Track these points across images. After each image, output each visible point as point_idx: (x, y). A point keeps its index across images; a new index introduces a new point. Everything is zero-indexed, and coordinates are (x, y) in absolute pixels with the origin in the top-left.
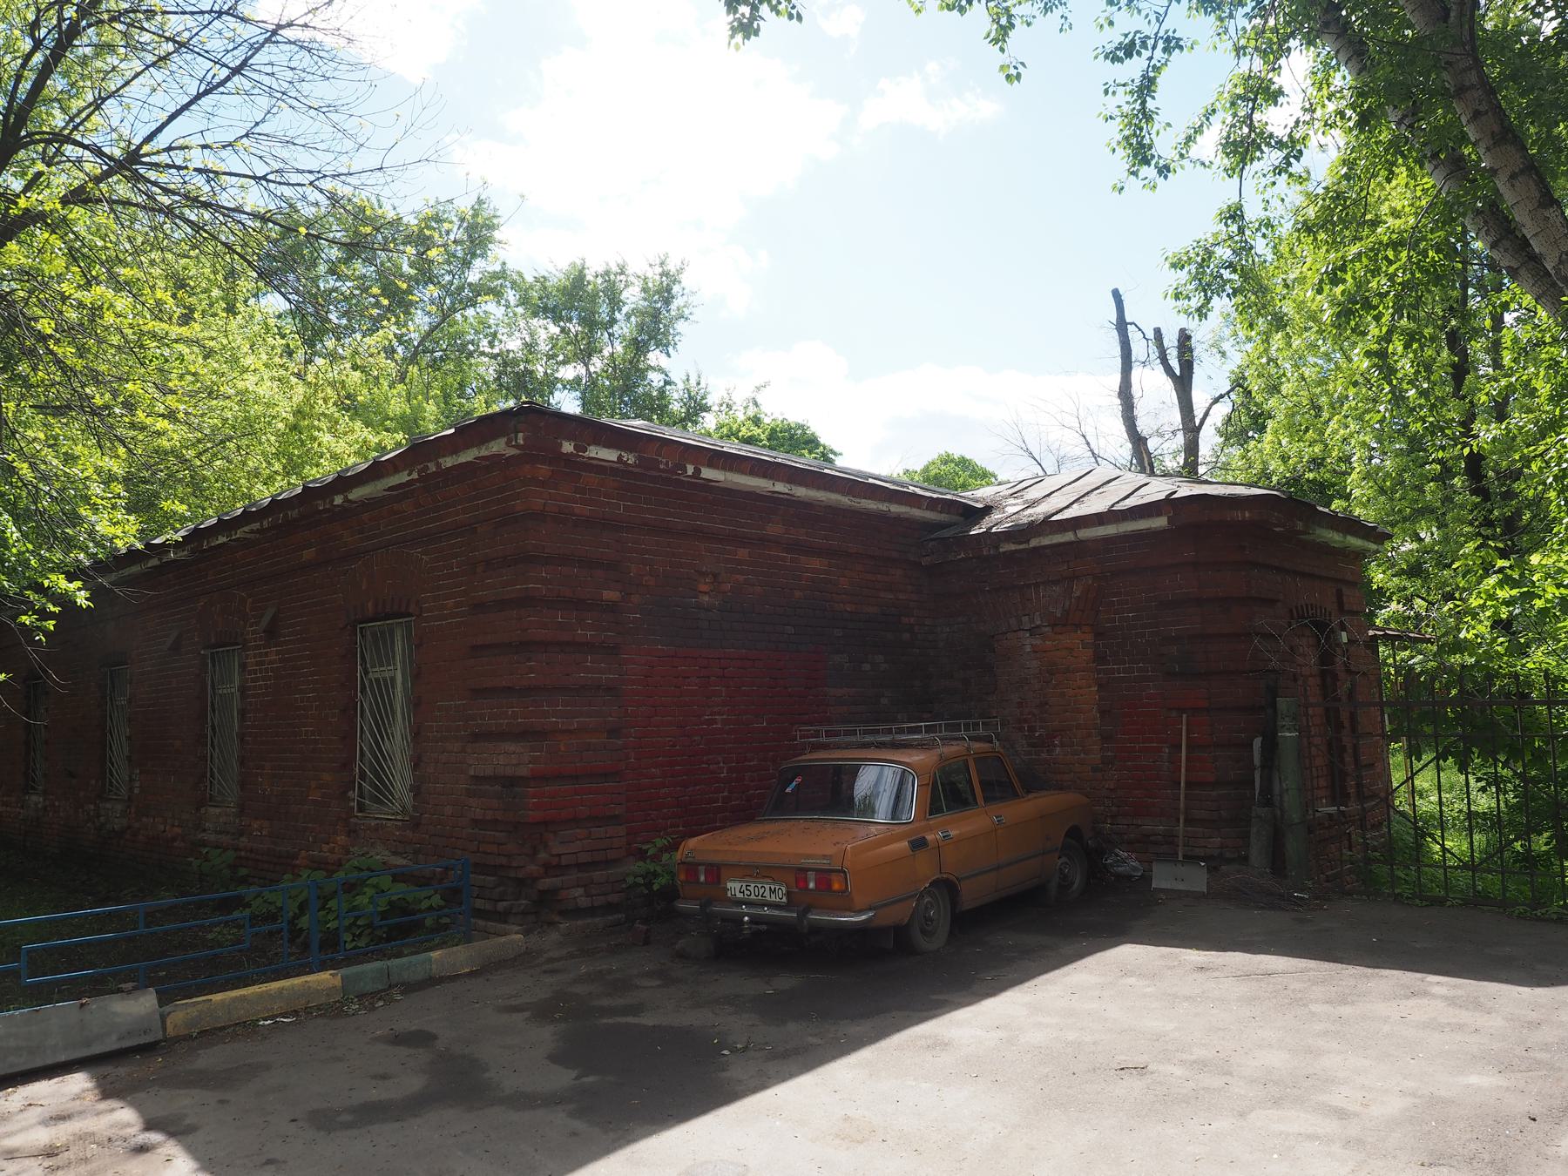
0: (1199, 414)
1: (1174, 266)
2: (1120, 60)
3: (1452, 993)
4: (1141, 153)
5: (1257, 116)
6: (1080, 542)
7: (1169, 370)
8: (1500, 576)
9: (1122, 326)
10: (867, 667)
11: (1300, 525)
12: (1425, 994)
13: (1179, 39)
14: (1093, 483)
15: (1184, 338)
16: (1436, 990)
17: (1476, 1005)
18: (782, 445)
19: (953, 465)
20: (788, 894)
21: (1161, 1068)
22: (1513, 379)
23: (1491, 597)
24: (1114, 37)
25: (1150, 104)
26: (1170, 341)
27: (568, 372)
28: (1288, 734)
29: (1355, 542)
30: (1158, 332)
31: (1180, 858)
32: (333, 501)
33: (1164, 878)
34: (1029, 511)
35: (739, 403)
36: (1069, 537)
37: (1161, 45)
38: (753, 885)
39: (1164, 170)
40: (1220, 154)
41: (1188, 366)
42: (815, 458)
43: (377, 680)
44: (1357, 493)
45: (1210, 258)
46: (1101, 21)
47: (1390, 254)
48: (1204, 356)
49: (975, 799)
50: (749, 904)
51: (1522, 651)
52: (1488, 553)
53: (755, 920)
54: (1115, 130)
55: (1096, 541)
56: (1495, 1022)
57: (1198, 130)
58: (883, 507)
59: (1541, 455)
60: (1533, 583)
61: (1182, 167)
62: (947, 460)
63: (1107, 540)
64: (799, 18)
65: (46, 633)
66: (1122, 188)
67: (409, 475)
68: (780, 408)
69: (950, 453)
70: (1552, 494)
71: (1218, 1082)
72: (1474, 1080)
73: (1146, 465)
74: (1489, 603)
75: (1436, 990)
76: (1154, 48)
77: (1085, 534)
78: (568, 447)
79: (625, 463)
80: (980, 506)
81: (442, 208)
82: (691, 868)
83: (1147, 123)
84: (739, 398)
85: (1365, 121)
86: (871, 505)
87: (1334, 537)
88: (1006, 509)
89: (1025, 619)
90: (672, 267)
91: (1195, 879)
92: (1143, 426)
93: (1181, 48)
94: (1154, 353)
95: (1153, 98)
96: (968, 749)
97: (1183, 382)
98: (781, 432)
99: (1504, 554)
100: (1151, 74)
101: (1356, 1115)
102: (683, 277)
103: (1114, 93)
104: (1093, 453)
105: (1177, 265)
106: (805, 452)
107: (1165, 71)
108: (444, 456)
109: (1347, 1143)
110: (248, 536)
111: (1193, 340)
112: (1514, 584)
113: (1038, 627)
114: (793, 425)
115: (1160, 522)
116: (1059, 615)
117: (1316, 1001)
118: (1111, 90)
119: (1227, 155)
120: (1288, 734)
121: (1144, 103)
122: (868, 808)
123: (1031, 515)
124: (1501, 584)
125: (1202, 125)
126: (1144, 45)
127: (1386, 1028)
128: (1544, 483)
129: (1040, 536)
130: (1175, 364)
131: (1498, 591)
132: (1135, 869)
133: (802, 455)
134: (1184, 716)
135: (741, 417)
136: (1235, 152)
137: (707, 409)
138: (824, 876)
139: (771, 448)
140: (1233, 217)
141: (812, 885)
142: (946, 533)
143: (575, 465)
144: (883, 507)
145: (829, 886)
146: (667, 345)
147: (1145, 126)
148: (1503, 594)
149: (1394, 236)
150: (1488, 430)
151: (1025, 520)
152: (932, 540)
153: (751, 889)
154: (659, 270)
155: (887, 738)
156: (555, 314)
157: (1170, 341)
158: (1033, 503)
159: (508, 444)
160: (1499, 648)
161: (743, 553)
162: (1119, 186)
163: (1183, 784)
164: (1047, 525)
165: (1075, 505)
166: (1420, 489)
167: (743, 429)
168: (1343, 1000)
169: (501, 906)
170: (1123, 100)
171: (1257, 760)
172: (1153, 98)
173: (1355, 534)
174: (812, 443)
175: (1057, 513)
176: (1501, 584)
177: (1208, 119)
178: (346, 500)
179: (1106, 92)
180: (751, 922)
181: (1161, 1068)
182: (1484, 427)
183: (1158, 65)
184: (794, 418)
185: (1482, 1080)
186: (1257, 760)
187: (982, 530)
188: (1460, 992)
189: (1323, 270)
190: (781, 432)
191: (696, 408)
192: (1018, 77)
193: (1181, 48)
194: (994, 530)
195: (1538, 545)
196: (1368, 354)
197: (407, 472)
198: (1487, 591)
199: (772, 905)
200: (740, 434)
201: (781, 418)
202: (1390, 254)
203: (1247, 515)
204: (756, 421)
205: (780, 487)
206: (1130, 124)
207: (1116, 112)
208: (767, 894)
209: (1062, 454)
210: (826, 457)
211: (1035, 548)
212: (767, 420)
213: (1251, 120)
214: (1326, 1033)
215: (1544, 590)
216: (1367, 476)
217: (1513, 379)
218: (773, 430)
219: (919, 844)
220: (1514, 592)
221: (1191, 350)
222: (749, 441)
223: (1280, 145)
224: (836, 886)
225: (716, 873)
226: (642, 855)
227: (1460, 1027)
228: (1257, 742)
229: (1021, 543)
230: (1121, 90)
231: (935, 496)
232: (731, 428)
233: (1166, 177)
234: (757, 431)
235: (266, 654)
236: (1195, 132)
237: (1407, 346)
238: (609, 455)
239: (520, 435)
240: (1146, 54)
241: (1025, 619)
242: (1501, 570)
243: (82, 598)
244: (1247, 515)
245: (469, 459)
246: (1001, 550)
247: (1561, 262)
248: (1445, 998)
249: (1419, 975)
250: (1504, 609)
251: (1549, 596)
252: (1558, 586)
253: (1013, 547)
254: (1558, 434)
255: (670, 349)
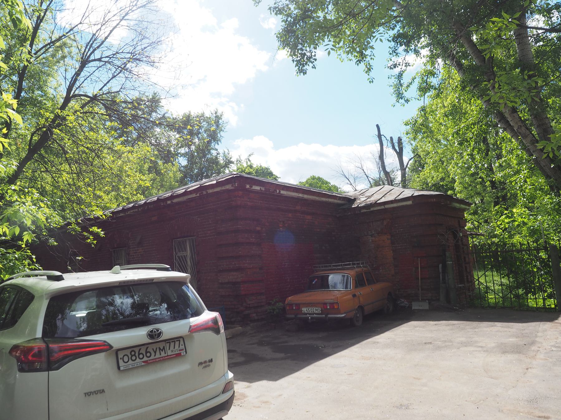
0: (405, 164)
1: (406, 125)
2: (392, 69)
3: (502, 325)
4: (400, 96)
5: (428, 80)
6: (386, 209)
7: (395, 150)
8: (506, 216)
9: (380, 136)
10: (324, 248)
11: (448, 202)
12: (495, 326)
13: (409, 63)
14: (386, 191)
15: (400, 140)
16: (498, 325)
17: (509, 327)
18: (260, 175)
19: (316, 180)
20: (322, 310)
21: (435, 342)
22: (506, 159)
23: (503, 221)
24: (391, 63)
25: (402, 82)
26: (395, 141)
27: (182, 151)
28: (449, 263)
29: (463, 206)
30: (391, 138)
31: (420, 300)
32: (167, 202)
33: (416, 306)
34: (368, 200)
35: (243, 160)
36: (382, 207)
37: (404, 65)
38: (310, 309)
39: (407, 101)
40: (418, 91)
41: (401, 149)
42: (272, 179)
43: (182, 256)
44: (457, 189)
45: (416, 122)
46: (388, 59)
47: (472, 126)
48: (406, 146)
49: (365, 283)
50: (309, 314)
51: (511, 237)
52: (502, 209)
53: (312, 318)
54: (392, 90)
55: (390, 208)
56: (514, 330)
57: (411, 83)
58: (327, 200)
59: (515, 180)
60: (515, 217)
61: (412, 100)
62: (313, 178)
63: (394, 208)
64: (315, 68)
65: (94, 244)
66: (395, 106)
67: (196, 195)
68: (258, 162)
69: (315, 175)
70: (519, 192)
71: (450, 344)
72: (511, 340)
73: (389, 181)
74: (503, 223)
75: (498, 325)
76: (402, 65)
77: (387, 206)
78: (248, 186)
79: (262, 190)
80: (353, 198)
81: (141, 96)
82: (291, 305)
83: (401, 87)
84: (243, 158)
85: (463, 88)
86: (324, 199)
87: (457, 205)
88: (361, 199)
89: (369, 232)
90: (218, 114)
91: (425, 306)
92: (388, 169)
93: (410, 66)
94: (390, 145)
95: (402, 79)
96: (363, 270)
97: (400, 154)
98: (260, 170)
99: (507, 209)
100: (402, 73)
101: (485, 347)
102: (223, 117)
103: (391, 78)
104: (367, 176)
105: (406, 124)
106: (268, 177)
107: (406, 72)
108: (209, 189)
109: (484, 351)
110: (131, 213)
111: (403, 141)
112: (510, 218)
113: (374, 234)
114: (264, 168)
115: (410, 203)
116: (380, 230)
117: (468, 329)
118: (390, 77)
119: (420, 92)
120: (449, 263)
121: (400, 81)
122: (335, 286)
123: (370, 201)
124: (506, 218)
125: (412, 82)
126: (399, 65)
127: (487, 332)
128: (516, 189)
129: (374, 207)
130: (397, 148)
131: (505, 220)
132: (406, 304)
133: (267, 178)
134: (419, 259)
135: (245, 165)
136: (422, 91)
137: (232, 163)
138: (332, 304)
139: (257, 176)
140: (422, 110)
141: (328, 307)
142: (345, 207)
143: (250, 191)
144: (327, 200)
145: (334, 307)
146: (218, 141)
147: (400, 88)
148: (506, 221)
149: (473, 122)
150: (500, 173)
151: (369, 203)
152: (340, 209)
153: (310, 310)
154: (215, 115)
155: (330, 268)
156: (179, 131)
157: (395, 141)
158: (369, 197)
159: (232, 186)
160: (506, 236)
161: (290, 215)
162: (394, 105)
163: (420, 278)
164: (376, 204)
165: (383, 198)
166: (475, 187)
167: (247, 170)
168: (475, 328)
169: (233, 320)
170: (394, 81)
171: (440, 270)
172: (402, 79)
173: (463, 204)
174: (271, 174)
175: (378, 200)
176: (506, 218)
177: (413, 80)
178: (172, 202)
179: (389, 78)
180: (311, 319)
181: (435, 342)
182: (499, 172)
183: (403, 70)
184: (264, 165)
185: (513, 340)
186: (440, 270)
187: (356, 206)
188: (504, 325)
189: (454, 131)
190: (260, 170)
191: (229, 162)
192: (372, 82)
193: (410, 66)
194: (359, 206)
195: (514, 205)
196: (468, 155)
197: (195, 194)
198: (502, 220)
199: (316, 314)
200: (246, 171)
201: (259, 165)
202: (472, 126)
203: (434, 200)
204: (251, 167)
205: (301, 195)
206: (396, 87)
207: (392, 84)
208: (315, 311)
209: (356, 176)
210: (276, 178)
211: (372, 211)
212: (254, 166)
213: (427, 81)
214: (473, 334)
215: (518, 219)
216: (460, 183)
217: (506, 159)
218: (257, 170)
219: (354, 296)
220: (509, 220)
221: (402, 144)
222: (249, 173)
223: (435, 89)
224: (336, 307)
225: (298, 306)
226: (269, 304)
227: (506, 331)
228: (440, 266)
229: (368, 209)
230: (393, 77)
231: (341, 196)
232: (242, 169)
233: (407, 103)
234: (251, 170)
235: (138, 250)
236: (410, 84)
237: (478, 153)
238: (257, 188)
239: (236, 184)
240: (400, 67)
241: (369, 232)
242: (506, 214)
243: (102, 234)
244: (434, 200)
245: (218, 190)
246: (362, 212)
247: (518, 128)
248: (501, 326)
249: (493, 323)
250: (507, 225)
251: (519, 221)
252: (522, 218)
253: (365, 211)
254: (519, 175)
255: (219, 143)
